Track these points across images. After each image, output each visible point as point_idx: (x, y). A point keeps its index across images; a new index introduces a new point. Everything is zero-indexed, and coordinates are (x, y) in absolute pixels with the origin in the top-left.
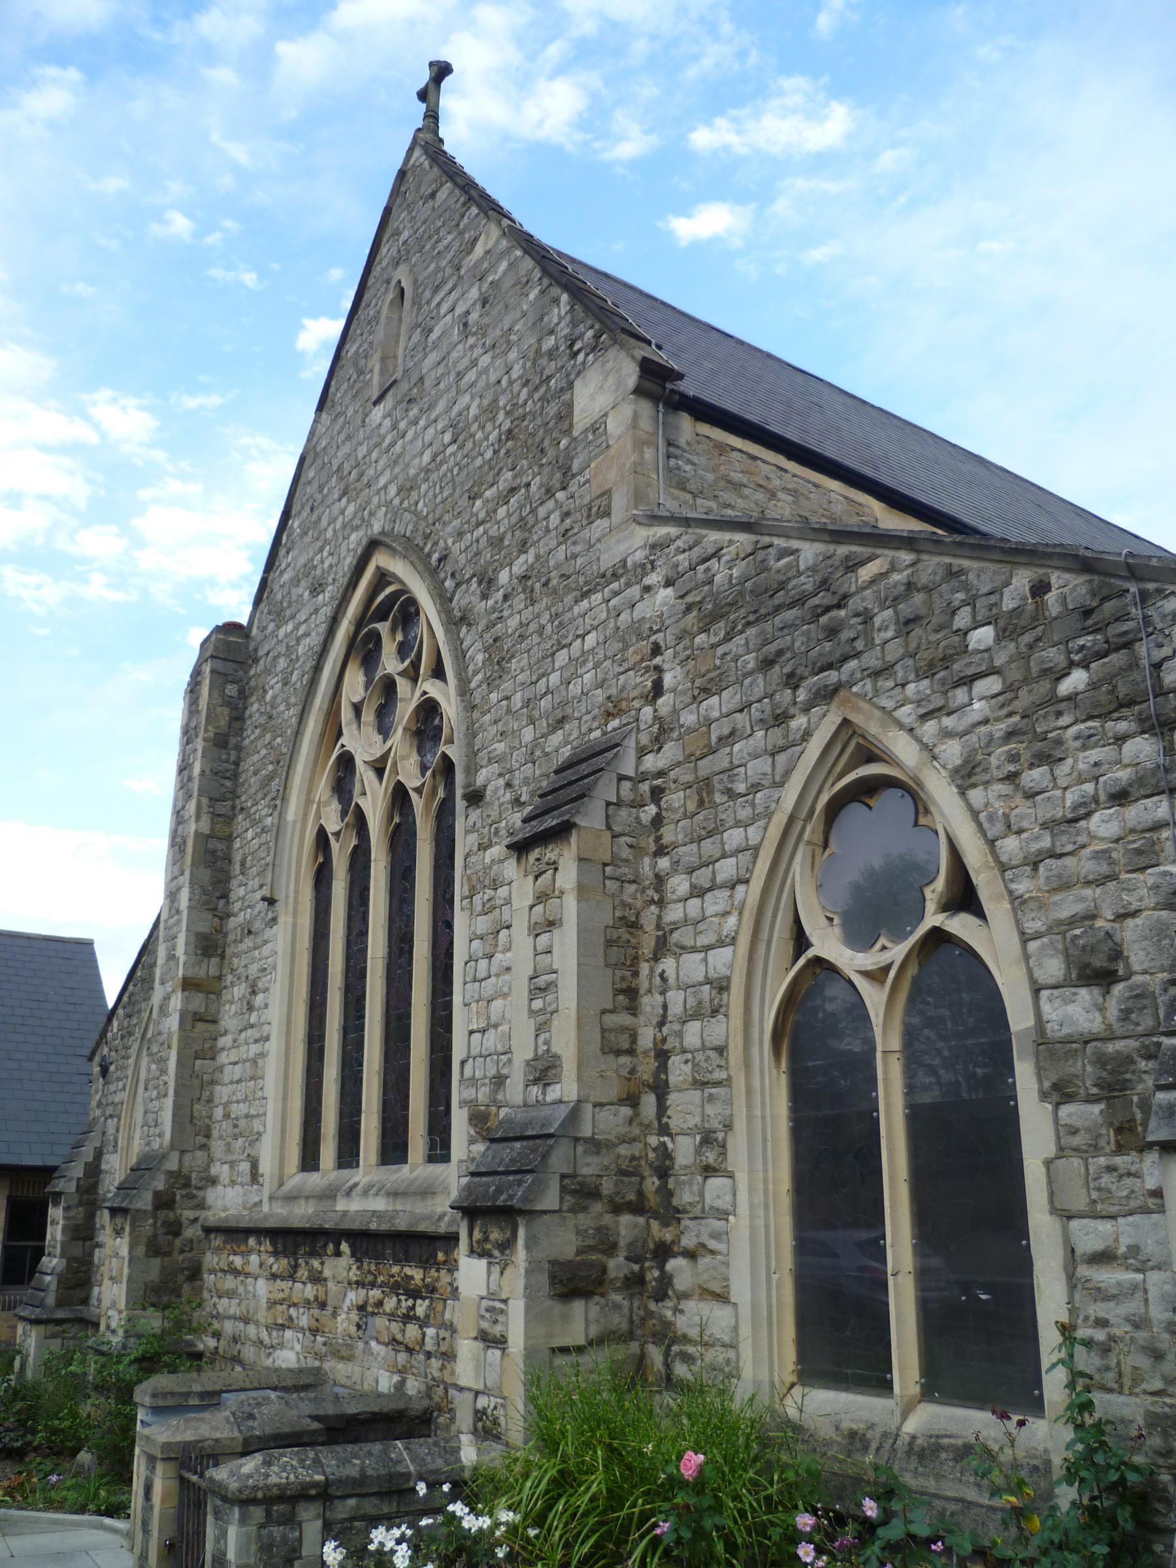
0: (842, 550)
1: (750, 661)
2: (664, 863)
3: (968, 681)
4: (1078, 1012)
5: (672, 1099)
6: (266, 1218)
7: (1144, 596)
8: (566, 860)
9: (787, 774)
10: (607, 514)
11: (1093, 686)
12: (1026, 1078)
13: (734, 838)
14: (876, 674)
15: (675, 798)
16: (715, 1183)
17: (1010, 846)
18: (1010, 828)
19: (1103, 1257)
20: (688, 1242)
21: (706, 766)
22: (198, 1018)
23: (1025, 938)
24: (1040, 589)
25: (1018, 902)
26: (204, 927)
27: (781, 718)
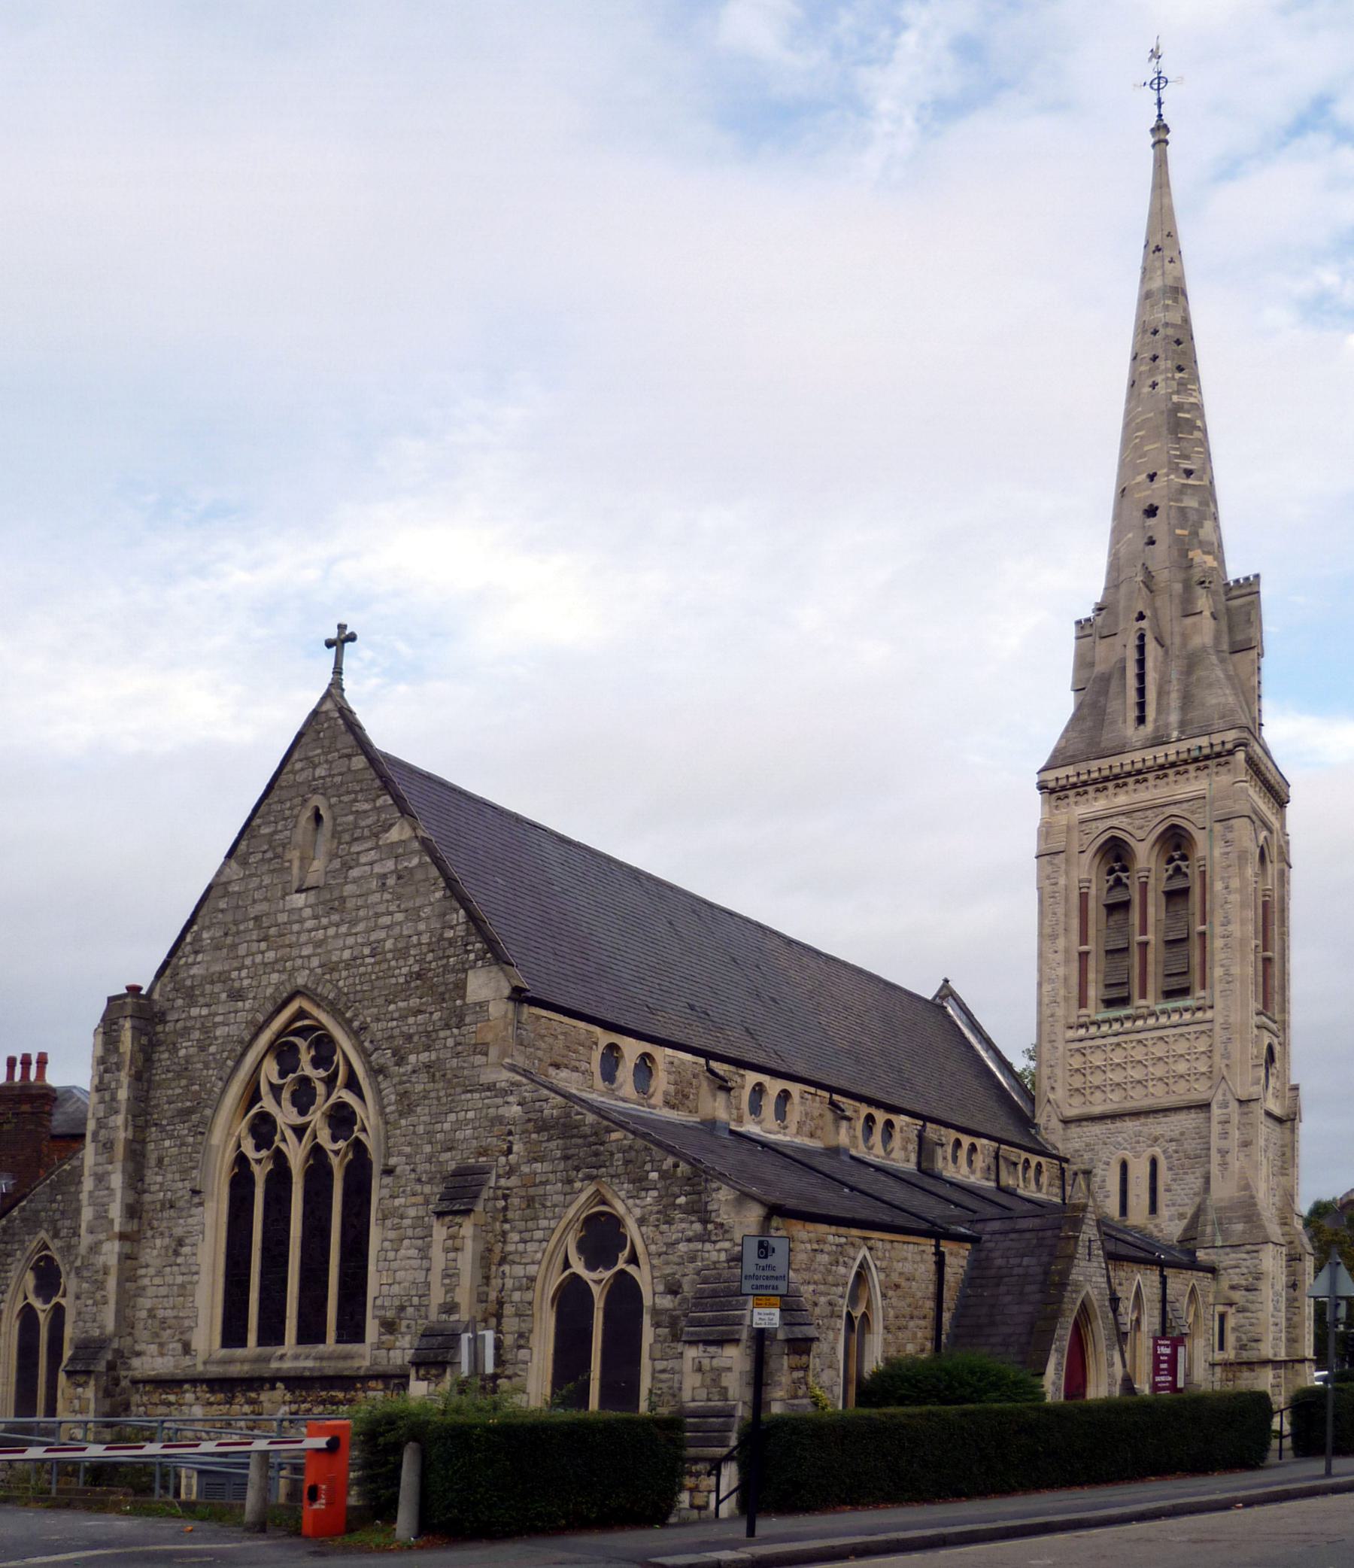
0: (606, 1123)
1: (558, 1154)
2: (507, 1226)
3: (647, 1190)
4: (666, 1302)
5: (505, 1320)
6: (201, 1373)
7: (706, 1181)
8: (467, 1228)
9: (571, 1204)
10: (486, 1054)
11: (687, 1203)
12: (647, 1320)
13: (543, 1223)
14: (612, 1176)
15: (515, 1201)
16: (522, 1351)
17: (653, 1248)
18: (654, 1242)
19: (663, 1371)
20: (507, 1373)
21: (532, 1191)
22: (128, 1257)
23: (653, 1278)
24: (676, 1166)
25: (653, 1267)
26: (130, 1201)
27: (570, 1182)
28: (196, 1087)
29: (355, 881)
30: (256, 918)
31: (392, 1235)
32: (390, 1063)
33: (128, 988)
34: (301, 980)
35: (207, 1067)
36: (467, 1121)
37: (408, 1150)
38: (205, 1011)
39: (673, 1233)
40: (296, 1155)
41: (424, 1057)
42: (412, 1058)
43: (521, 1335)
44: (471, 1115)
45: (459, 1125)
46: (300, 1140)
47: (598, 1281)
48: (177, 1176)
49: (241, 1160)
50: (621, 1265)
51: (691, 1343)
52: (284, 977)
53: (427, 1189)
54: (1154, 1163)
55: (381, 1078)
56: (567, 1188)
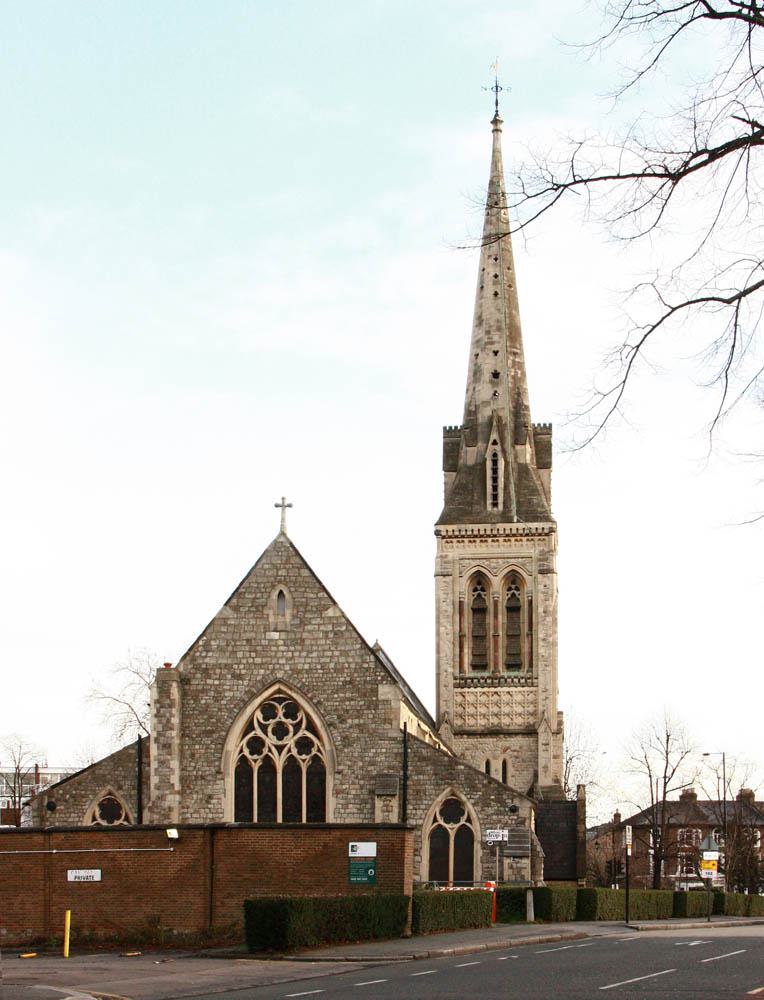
21: (418, 787)
28: (214, 720)
29: (309, 632)
30: (248, 640)
31: (342, 802)
32: (337, 722)
33: (165, 664)
34: (279, 675)
35: (220, 710)
36: (382, 753)
37: (349, 763)
38: (217, 682)
39: (490, 811)
40: (280, 762)
41: (356, 721)
42: (349, 721)
43: (416, 850)
44: (384, 750)
45: (377, 754)
46: (280, 755)
47: (452, 829)
48: (205, 764)
49: (243, 759)
50: (462, 822)
51: (508, 857)
52: (268, 672)
53: (362, 782)
54: (505, 763)
55: (332, 728)
56: (437, 788)
